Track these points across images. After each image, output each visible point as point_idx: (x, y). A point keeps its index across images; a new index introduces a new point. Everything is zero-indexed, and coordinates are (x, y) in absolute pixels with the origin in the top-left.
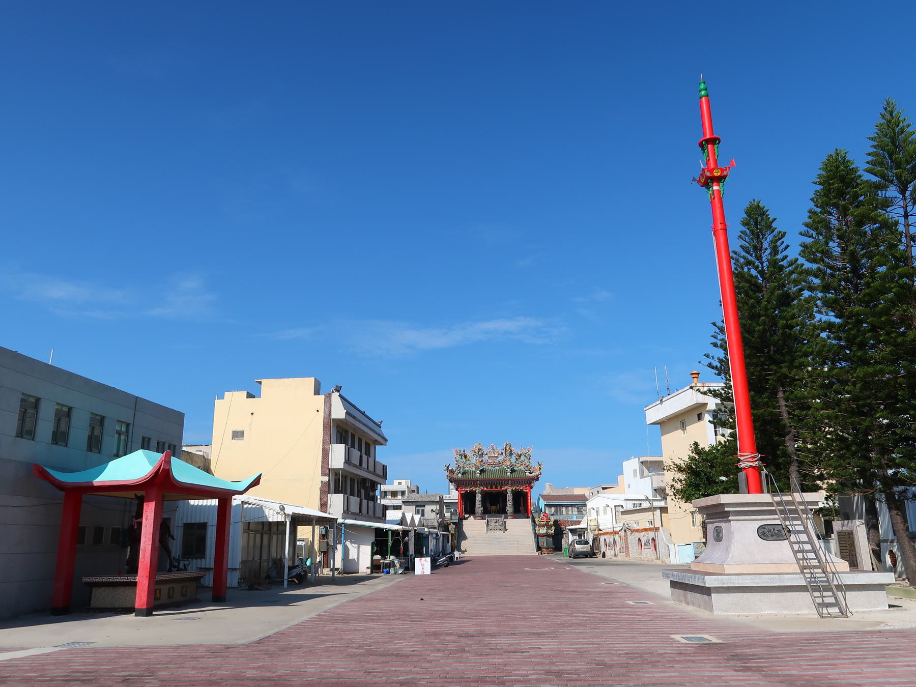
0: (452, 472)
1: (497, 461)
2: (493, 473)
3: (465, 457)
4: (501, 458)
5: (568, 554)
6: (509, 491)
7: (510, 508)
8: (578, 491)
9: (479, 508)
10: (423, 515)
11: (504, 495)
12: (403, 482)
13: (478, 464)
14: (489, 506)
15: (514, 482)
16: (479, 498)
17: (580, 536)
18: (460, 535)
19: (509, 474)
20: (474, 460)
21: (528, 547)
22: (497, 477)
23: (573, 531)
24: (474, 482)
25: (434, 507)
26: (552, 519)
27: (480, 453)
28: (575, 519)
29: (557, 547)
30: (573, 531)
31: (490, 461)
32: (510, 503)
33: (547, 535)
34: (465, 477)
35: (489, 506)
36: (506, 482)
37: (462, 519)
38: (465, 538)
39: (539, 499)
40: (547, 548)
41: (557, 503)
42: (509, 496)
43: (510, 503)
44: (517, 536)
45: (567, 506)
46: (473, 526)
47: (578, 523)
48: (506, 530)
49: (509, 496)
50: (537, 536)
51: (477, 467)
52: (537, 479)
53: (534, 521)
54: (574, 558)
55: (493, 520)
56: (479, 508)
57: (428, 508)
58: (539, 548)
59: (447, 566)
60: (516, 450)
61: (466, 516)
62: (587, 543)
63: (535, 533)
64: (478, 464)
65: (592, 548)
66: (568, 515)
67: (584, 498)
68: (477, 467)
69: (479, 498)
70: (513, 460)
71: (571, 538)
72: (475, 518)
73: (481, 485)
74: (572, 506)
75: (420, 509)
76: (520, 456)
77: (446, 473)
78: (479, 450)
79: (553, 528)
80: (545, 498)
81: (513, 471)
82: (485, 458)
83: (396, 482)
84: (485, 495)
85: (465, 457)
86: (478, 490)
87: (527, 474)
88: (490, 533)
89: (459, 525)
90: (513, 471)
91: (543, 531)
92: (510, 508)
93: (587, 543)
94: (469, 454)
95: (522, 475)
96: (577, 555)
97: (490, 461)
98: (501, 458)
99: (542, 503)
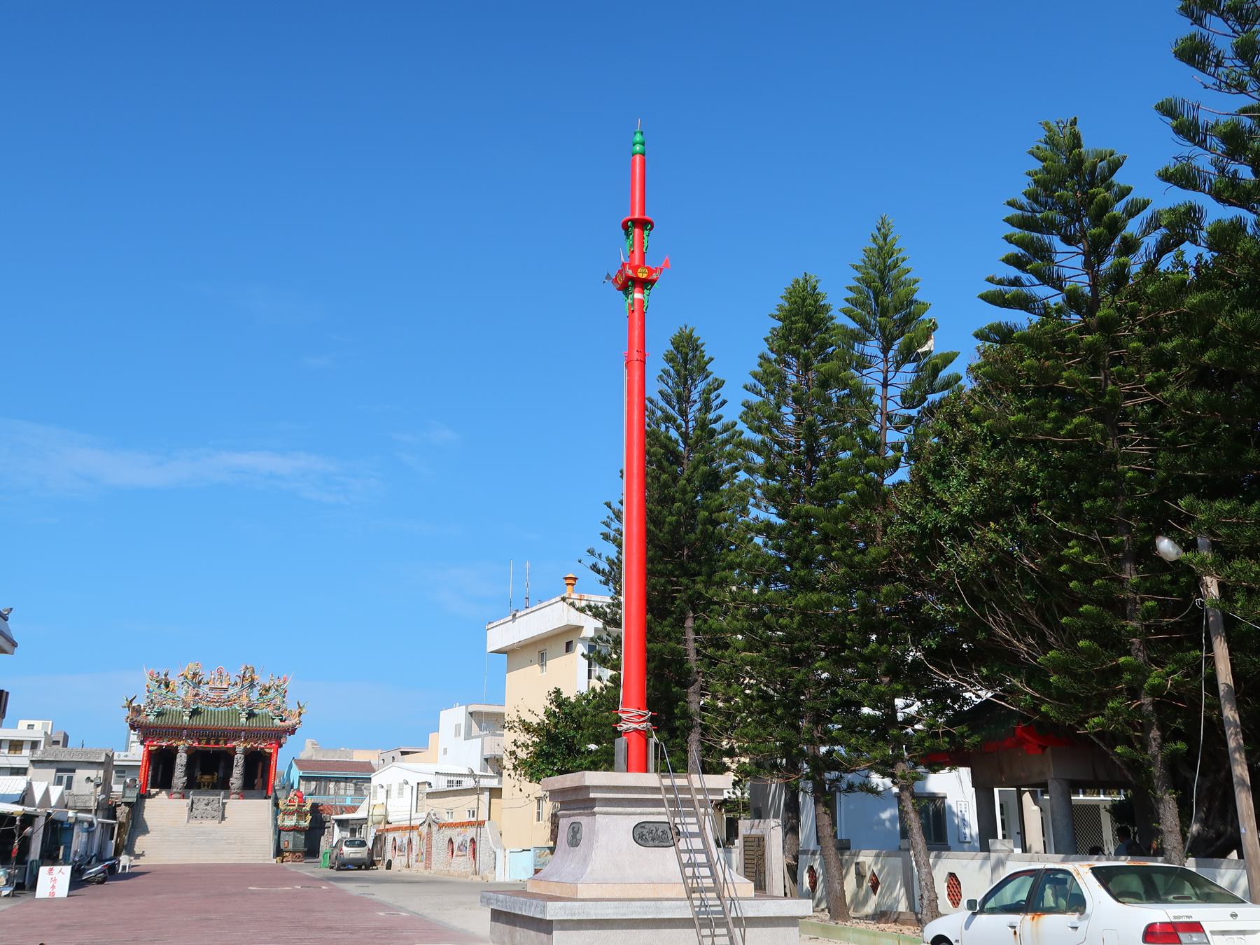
0: (137, 711)
1: (224, 696)
2: (215, 717)
3: (167, 685)
4: (232, 691)
5: (328, 863)
7: (236, 780)
8: (359, 756)
9: (179, 777)
10: (69, 787)
11: (228, 756)
12: (38, 725)
13: (189, 699)
14: (198, 774)
15: (251, 734)
16: (181, 759)
17: (353, 832)
18: (136, 825)
19: (243, 720)
20: (183, 692)
21: (260, 850)
22: (222, 723)
23: (342, 824)
24: (177, 732)
25: (92, 773)
26: (310, 801)
27: (196, 680)
28: (348, 802)
29: (311, 851)
30: (342, 824)
31: (212, 695)
32: (237, 772)
33: (295, 829)
34: (161, 721)
35: (198, 774)
36: (235, 734)
37: (143, 797)
38: (145, 831)
39: (291, 766)
40: (294, 852)
41: (319, 775)
42: (239, 759)
43: (237, 772)
44: (243, 828)
45: (338, 780)
46: (164, 810)
47: (353, 809)
48: (223, 818)
49: (239, 759)
50: (279, 831)
51: (186, 705)
52: (292, 731)
53: (276, 805)
54: (339, 869)
55: (202, 800)
56: (179, 777)
57: (80, 775)
58: (279, 852)
59: (102, 882)
60: (262, 680)
61: (153, 791)
62: (363, 844)
63: (276, 825)
64: (189, 699)
65: (371, 852)
66: (337, 796)
67: (368, 768)
68: (186, 705)
69: (181, 759)
70: (255, 695)
71: (337, 834)
72: (170, 795)
74: (346, 780)
75: (65, 775)
76: (267, 690)
77: (127, 713)
78: (195, 675)
79: (309, 817)
80: (301, 764)
81: (251, 715)
82: (204, 689)
83: (23, 724)
84: (193, 755)
85: (167, 685)
86: (182, 745)
87: (277, 721)
88: (194, 823)
89: (136, 808)
90: (251, 715)
91: (290, 822)
92: (236, 780)
93: (363, 844)
94: (175, 680)
95: (266, 724)
96: (345, 865)
97: (212, 695)
98: (232, 691)
99: (296, 774)
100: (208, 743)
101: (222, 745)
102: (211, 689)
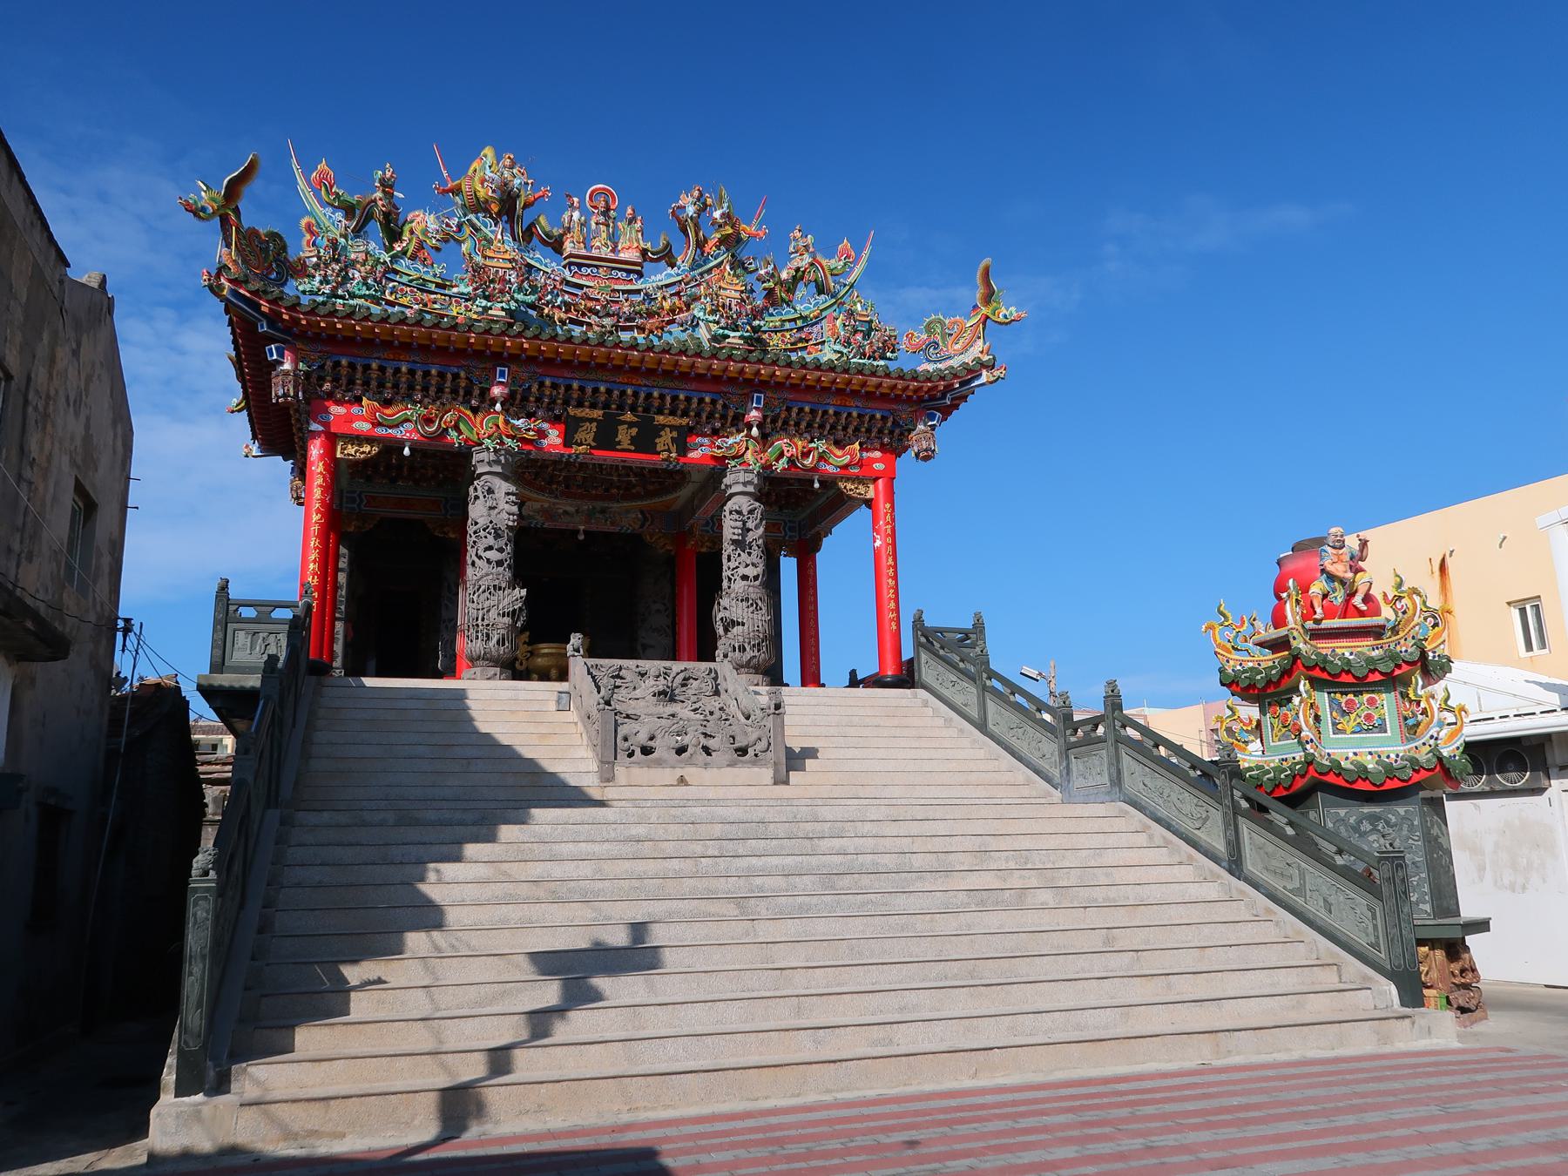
6: (738, 481)
16: (492, 506)
73: (515, 404)
86: (486, 433)
100: (605, 438)
101: (665, 452)
102: (576, 263)
